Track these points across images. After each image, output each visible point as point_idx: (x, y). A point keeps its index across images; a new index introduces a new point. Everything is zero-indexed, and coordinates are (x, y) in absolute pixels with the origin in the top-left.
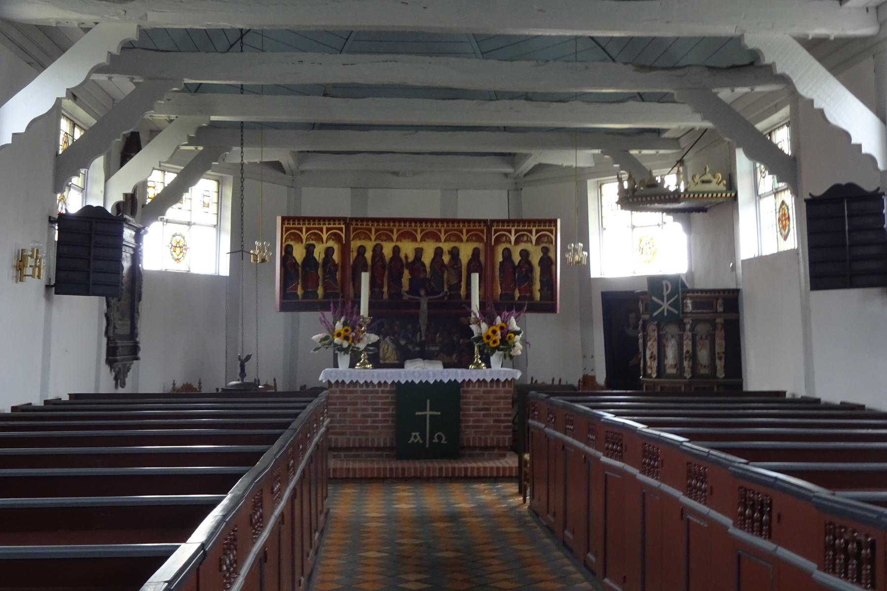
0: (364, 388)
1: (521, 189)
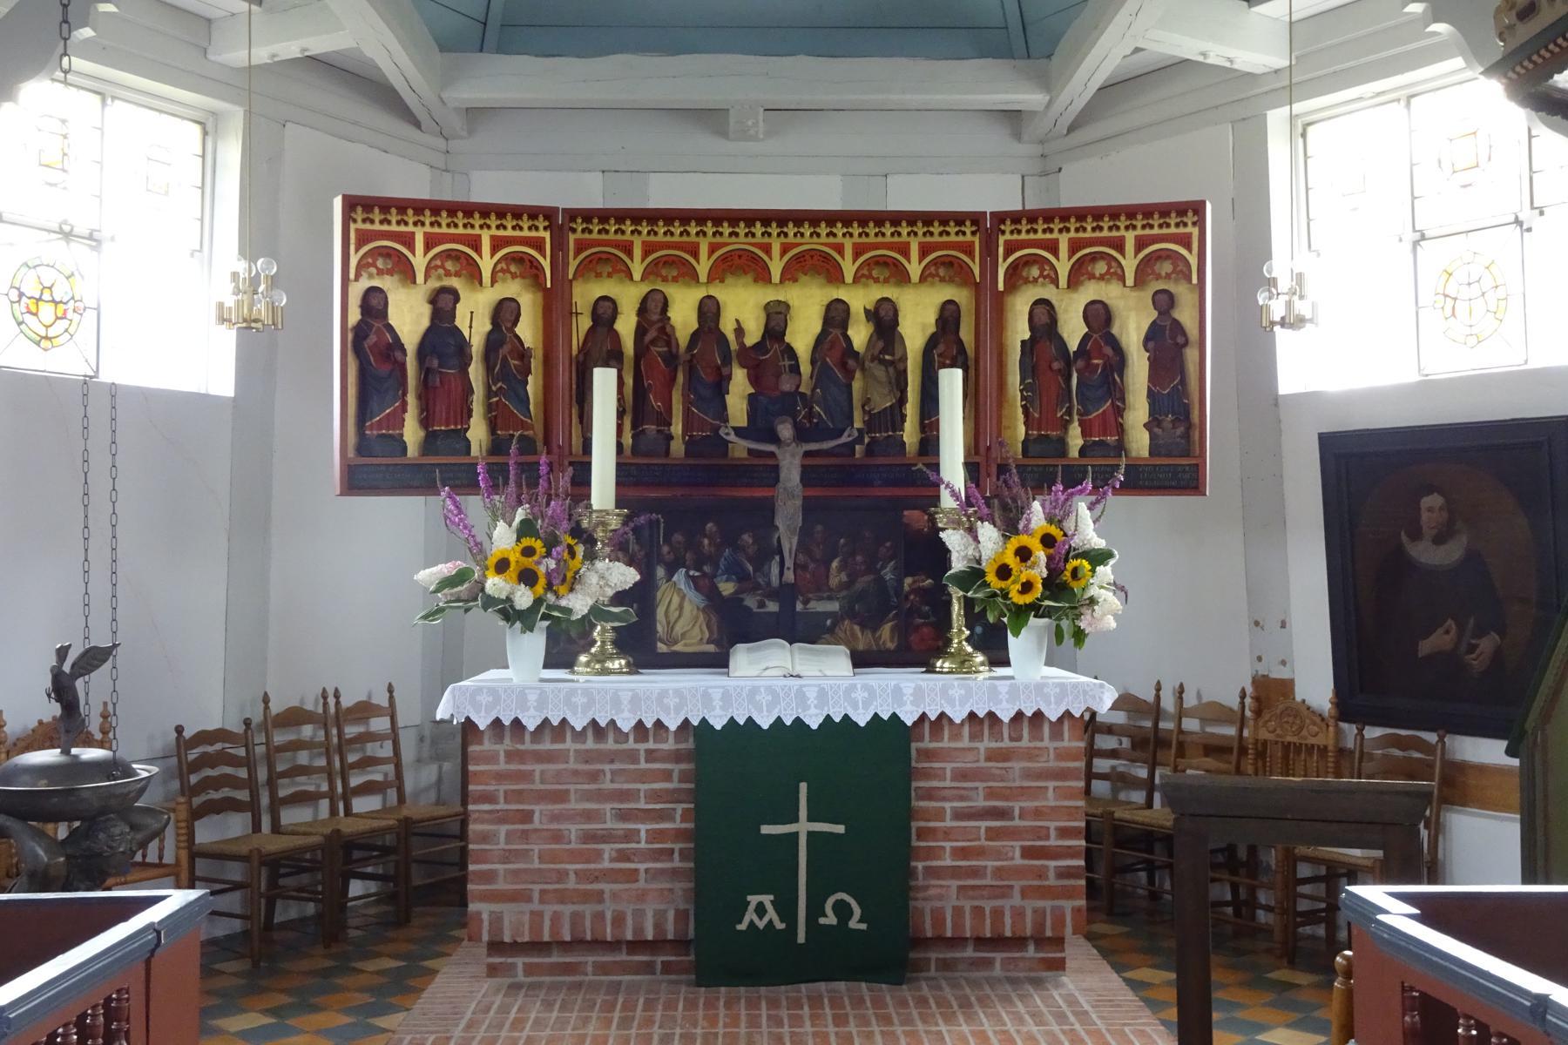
0: (590, 744)
1: (1060, 170)
